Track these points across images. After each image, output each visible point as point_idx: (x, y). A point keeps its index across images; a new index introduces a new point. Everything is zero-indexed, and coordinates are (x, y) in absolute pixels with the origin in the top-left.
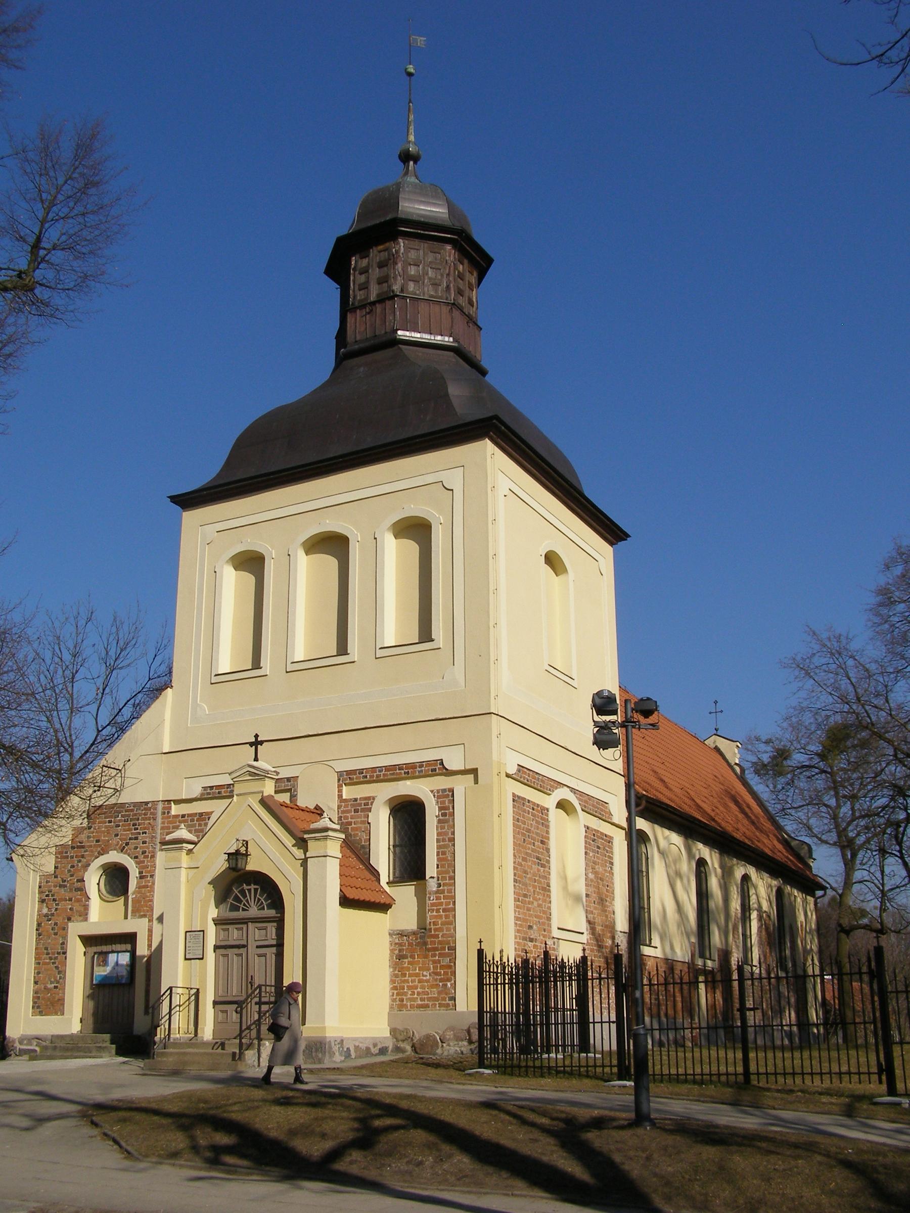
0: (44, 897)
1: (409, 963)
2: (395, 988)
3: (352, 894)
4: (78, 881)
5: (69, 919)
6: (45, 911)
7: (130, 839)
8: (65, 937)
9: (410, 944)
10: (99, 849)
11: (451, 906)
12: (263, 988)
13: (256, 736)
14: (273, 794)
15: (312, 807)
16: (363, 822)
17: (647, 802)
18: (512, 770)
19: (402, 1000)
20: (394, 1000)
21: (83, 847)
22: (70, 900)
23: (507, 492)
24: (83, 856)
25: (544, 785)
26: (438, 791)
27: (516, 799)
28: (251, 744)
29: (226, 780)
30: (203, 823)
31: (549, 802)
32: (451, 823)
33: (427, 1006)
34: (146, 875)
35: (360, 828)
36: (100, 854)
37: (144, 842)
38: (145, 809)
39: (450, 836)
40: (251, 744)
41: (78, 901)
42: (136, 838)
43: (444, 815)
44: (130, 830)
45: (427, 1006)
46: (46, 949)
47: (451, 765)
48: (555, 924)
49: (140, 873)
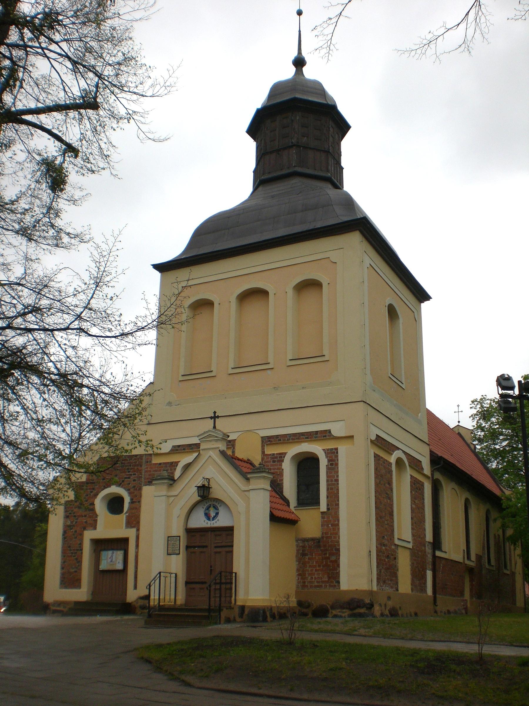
0: (68, 515)
1: (309, 559)
2: (299, 575)
3: (277, 513)
4: (91, 504)
5: (85, 529)
6: (69, 523)
7: (126, 478)
8: (82, 540)
9: (310, 547)
10: (104, 484)
11: (337, 522)
12: (223, 574)
13: (215, 413)
14: (225, 449)
15: (246, 459)
16: (278, 469)
17: (444, 462)
18: (374, 438)
19: (304, 582)
20: (299, 582)
21: (94, 483)
22: (85, 516)
23: (369, 266)
24: (94, 489)
25: (390, 448)
26: (328, 450)
27: (376, 456)
28: (211, 418)
29: (196, 441)
30: (173, 468)
31: (392, 459)
32: (336, 470)
33: (321, 586)
34: (136, 501)
35: (277, 472)
36: (105, 488)
37: (134, 480)
38: (135, 459)
39: (336, 478)
40: (211, 418)
41: (90, 517)
42: (129, 478)
43: (332, 464)
44: (125, 472)
45: (321, 586)
46: (70, 547)
47: (335, 433)
48: (396, 537)
49: (132, 499)
